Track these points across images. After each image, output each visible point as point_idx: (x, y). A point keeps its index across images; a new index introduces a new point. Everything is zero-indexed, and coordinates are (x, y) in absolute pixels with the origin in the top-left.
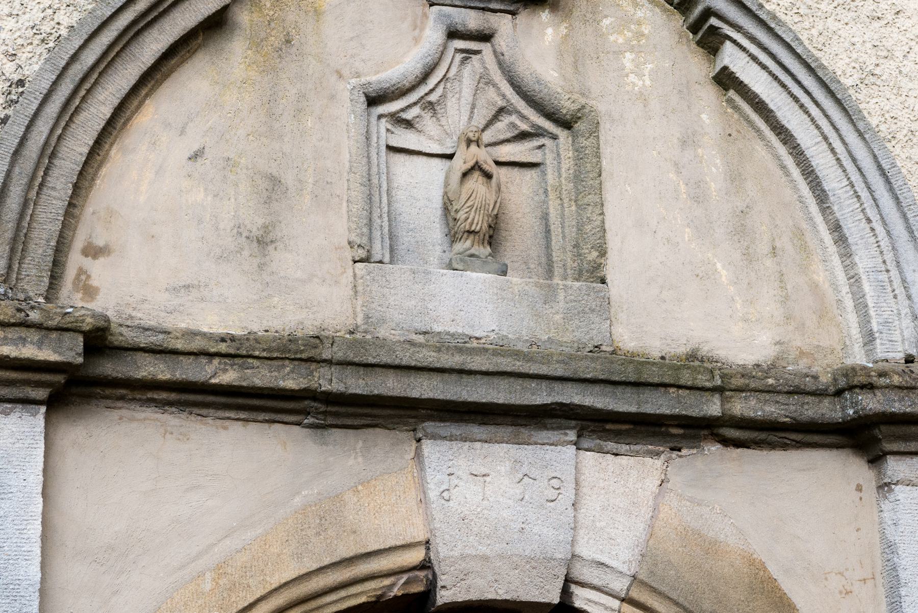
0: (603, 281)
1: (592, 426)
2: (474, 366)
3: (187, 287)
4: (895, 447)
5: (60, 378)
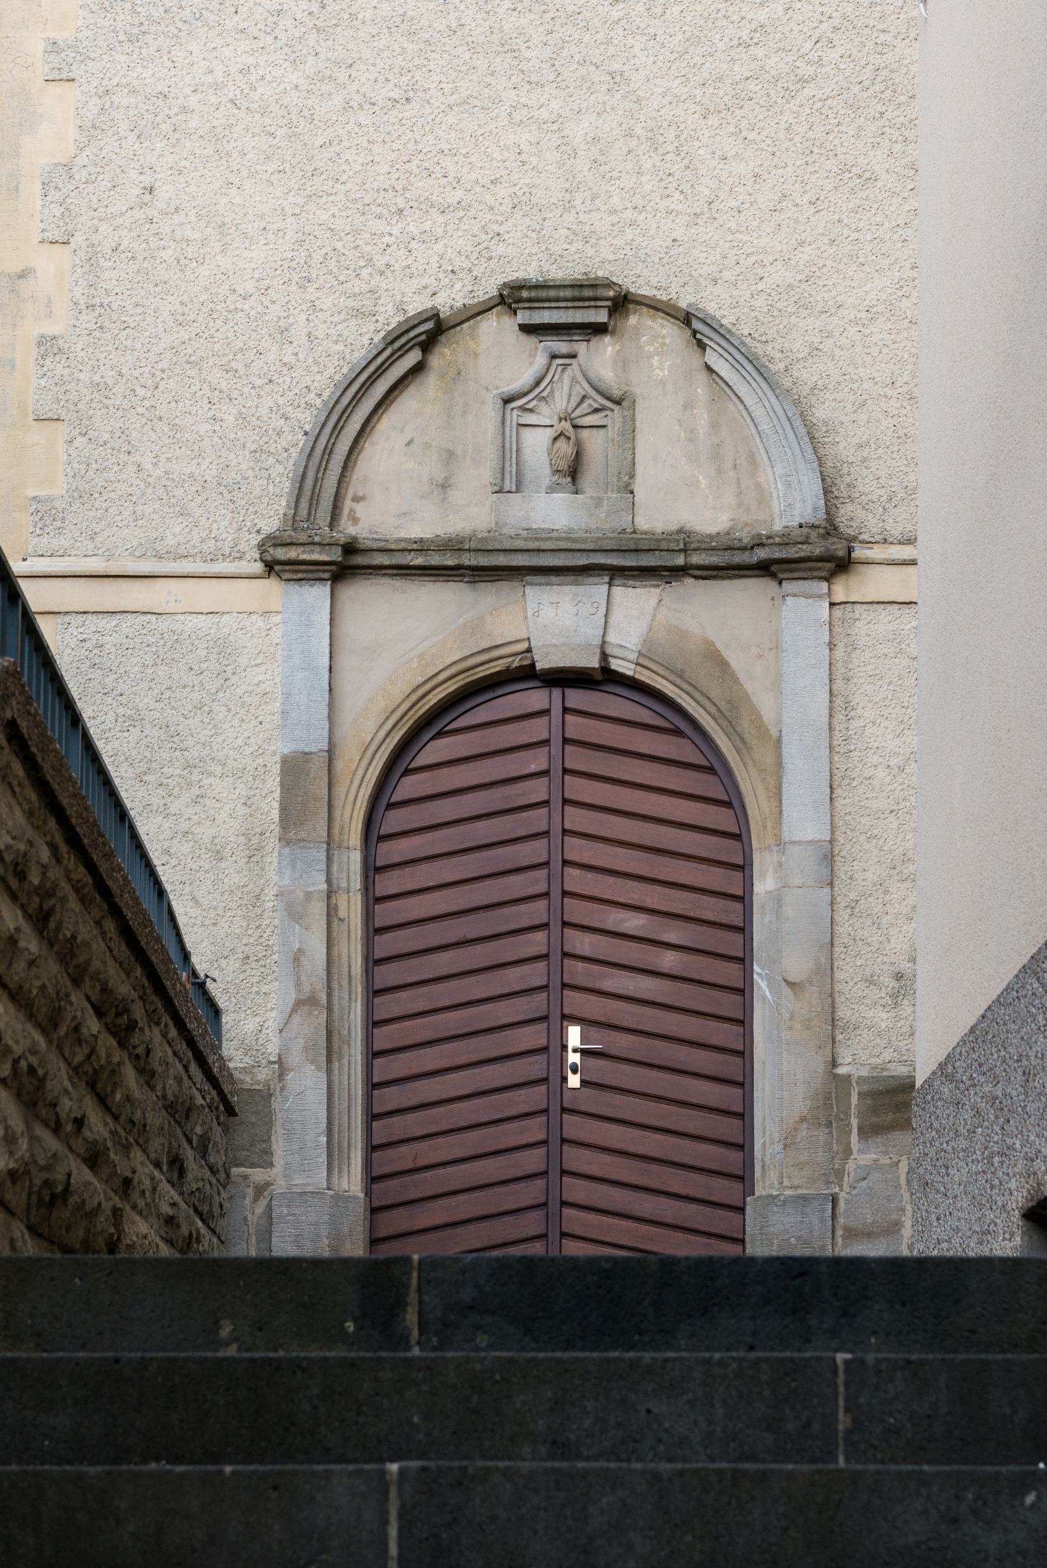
0: (632, 492)
1: (618, 573)
2: (545, 547)
3: (405, 514)
4: (786, 576)
5: (333, 568)
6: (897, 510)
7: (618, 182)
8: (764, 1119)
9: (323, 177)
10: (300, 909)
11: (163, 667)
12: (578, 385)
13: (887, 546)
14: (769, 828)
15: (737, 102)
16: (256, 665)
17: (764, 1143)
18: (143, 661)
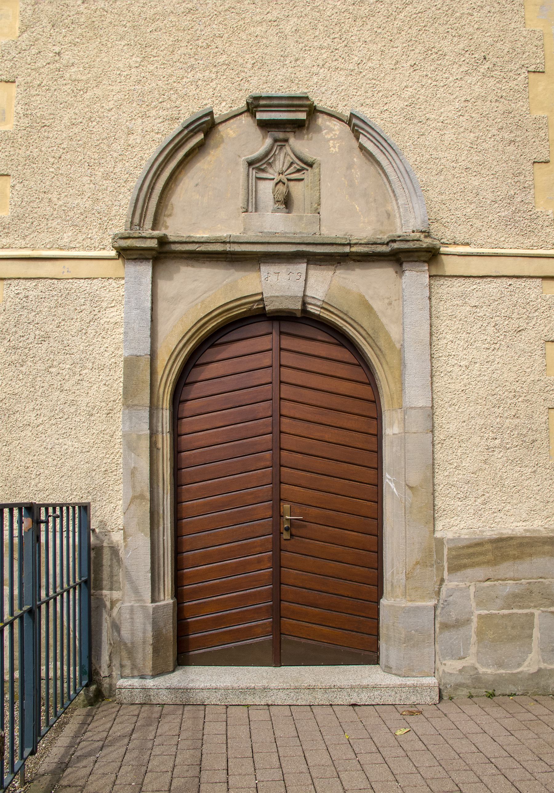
0: (319, 213)
6: (461, 227)
7: (309, 52)
8: (393, 560)
9: (152, 48)
10: (134, 444)
11: (60, 308)
12: (288, 157)
13: (455, 246)
14: (395, 399)
15: (371, 13)
16: (111, 307)
17: (393, 573)
18: (50, 305)
